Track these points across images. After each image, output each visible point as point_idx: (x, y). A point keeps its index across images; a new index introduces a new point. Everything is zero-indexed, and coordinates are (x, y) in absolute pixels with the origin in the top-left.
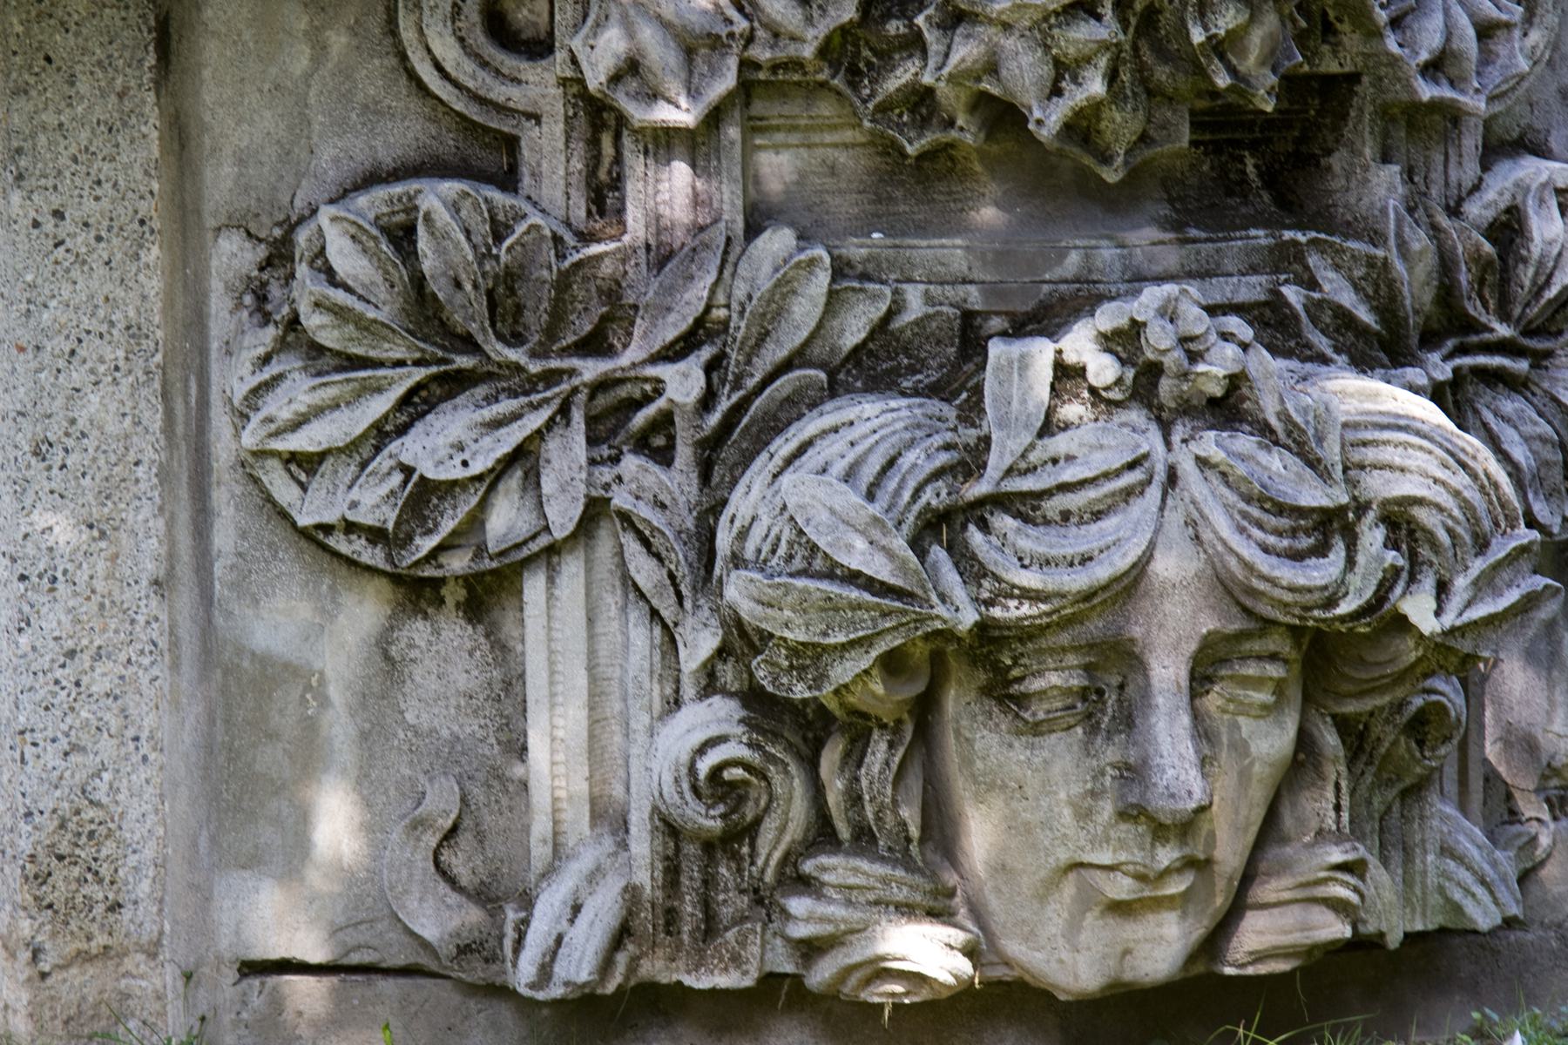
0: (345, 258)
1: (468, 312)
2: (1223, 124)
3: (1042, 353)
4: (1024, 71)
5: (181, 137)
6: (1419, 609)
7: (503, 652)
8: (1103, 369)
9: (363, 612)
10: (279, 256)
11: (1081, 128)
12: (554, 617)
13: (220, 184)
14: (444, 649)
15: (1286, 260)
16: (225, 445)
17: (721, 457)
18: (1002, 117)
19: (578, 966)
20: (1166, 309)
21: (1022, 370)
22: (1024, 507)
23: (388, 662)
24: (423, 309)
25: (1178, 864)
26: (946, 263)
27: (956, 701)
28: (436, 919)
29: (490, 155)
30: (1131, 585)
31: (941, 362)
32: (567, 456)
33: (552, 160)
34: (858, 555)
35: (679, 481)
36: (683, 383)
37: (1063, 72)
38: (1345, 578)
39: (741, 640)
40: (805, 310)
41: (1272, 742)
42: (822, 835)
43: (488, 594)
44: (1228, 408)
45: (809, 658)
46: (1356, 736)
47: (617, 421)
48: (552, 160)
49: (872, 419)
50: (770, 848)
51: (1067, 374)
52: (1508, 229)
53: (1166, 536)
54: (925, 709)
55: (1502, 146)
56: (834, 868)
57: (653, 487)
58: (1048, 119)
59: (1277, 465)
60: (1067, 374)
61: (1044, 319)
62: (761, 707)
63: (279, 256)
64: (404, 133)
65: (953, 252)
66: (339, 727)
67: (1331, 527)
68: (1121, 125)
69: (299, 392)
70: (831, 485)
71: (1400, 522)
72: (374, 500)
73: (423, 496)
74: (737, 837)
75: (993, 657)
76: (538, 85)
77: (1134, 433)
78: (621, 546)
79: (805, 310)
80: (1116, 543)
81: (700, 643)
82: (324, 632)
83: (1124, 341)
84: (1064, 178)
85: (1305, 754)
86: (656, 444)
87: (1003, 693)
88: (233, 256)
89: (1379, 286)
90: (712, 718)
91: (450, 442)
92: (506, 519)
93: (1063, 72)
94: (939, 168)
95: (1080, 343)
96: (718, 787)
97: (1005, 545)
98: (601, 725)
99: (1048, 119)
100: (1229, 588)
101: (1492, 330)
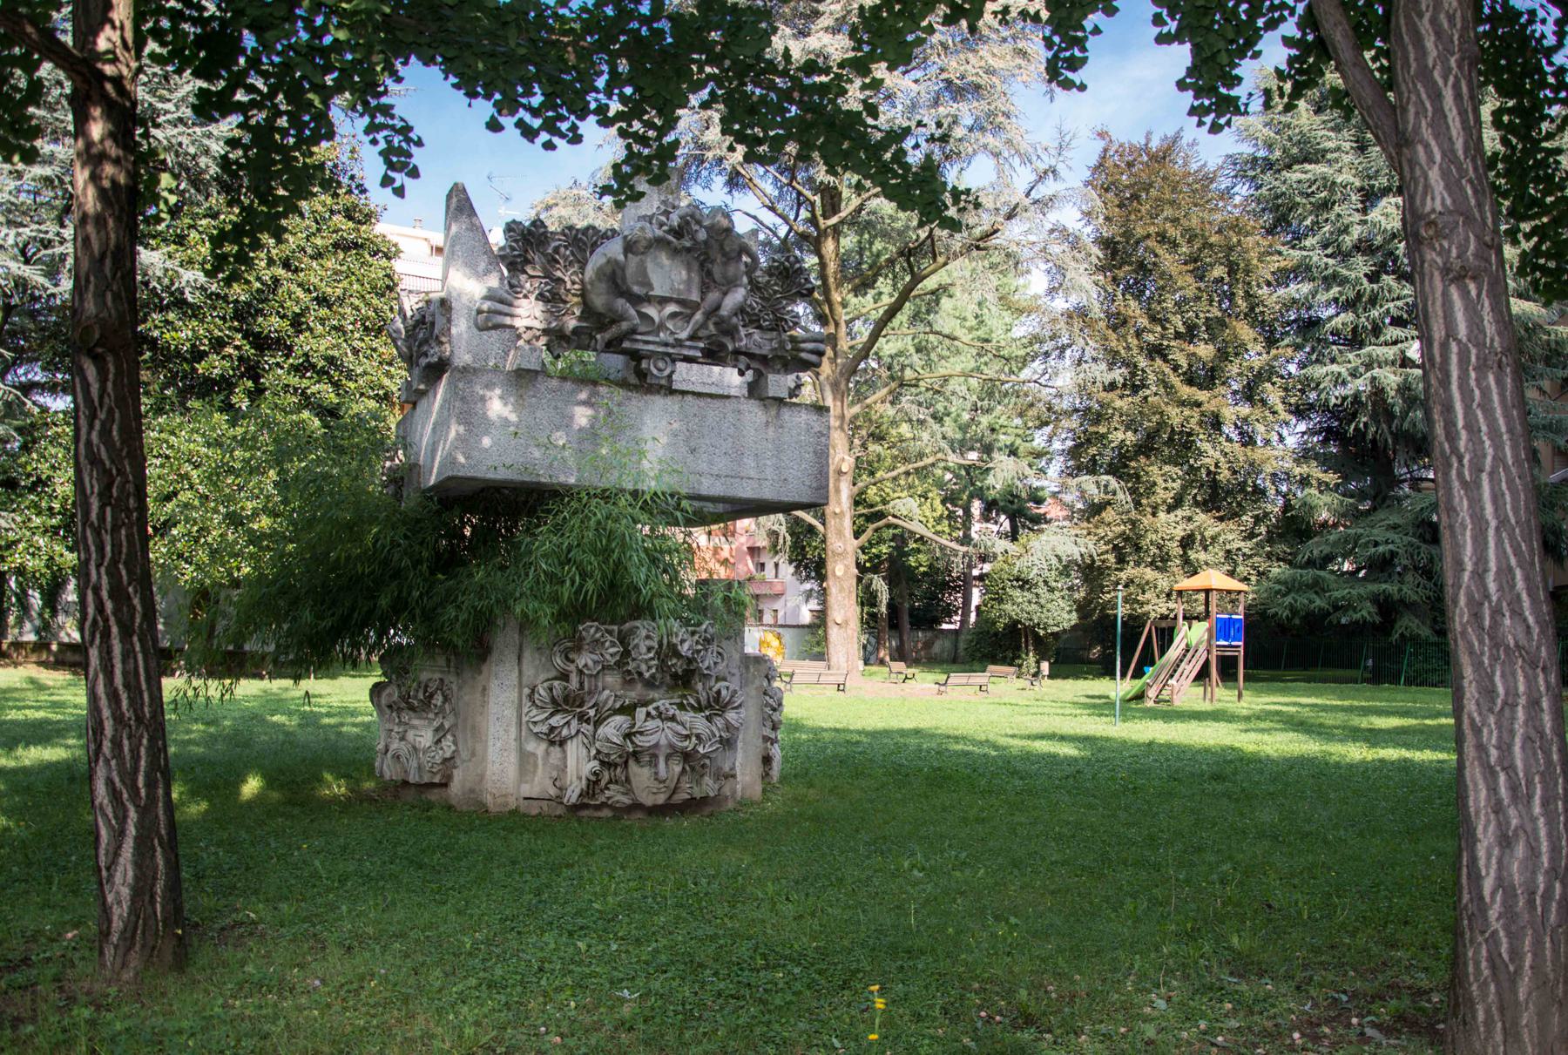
0: (542, 692)
1: (560, 700)
2: (675, 676)
3: (644, 710)
4: (643, 667)
5: (520, 672)
6: (701, 750)
7: (564, 752)
8: (654, 713)
9: (544, 746)
10: (533, 691)
11: (653, 676)
12: (573, 748)
13: (525, 680)
14: (556, 750)
15: (684, 696)
16: (525, 719)
17: (598, 723)
18: (640, 674)
19: (573, 800)
20: (663, 704)
21: (641, 713)
22: (641, 733)
23: (547, 753)
24: (554, 701)
25: (439, 610)
26: (632, 695)
27: (631, 763)
28: (553, 792)
29: (564, 677)
30: (657, 745)
31: (628, 710)
32: (574, 723)
33: (574, 679)
34: (615, 740)
35: (591, 727)
36: (592, 713)
37: (649, 668)
38: (689, 745)
39: (598, 752)
40: (610, 702)
41: (678, 769)
42: (610, 782)
43: (562, 743)
44: (673, 719)
45: (608, 755)
46: (693, 769)
47: (583, 718)
48: (574, 679)
49: (619, 719)
50: (603, 783)
51: (648, 714)
52: (719, 692)
53: (657, 734)
54: (626, 763)
55: (718, 679)
56: (612, 786)
57: (587, 728)
58: (647, 675)
59: (679, 728)
60: (648, 714)
61: (645, 704)
62: (602, 763)
63: (533, 691)
64: (553, 674)
65: (633, 694)
66: (540, 762)
67: (687, 737)
68: (658, 676)
69: (534, 712)
70: (612, 729)
71: (698, 737)
72: (545, 729)
73: (552, 729)
74: (597, 782)
75: (636, 755)
76: (572, 667)
77: (658, 722)
78: (775, 399)
79: (610, 702)
80: (652, 740)
81: (593, 752)
82: (538, 748)
83: (657, 708)
84: (650, 684)
85: (684, 771)
86: (588, 721)
87: (637, 761)
88: (526, 691)
89: (699, 702)
90: (595, 764)
91: (557, 720)
92: (565, 732)
93: (649, 668)
94: (632, 681)
95: (650, 708)
96: (595, 773)
97: (638, 740)
98: (578, 763)
99: (647, 675)
100: (671, 746)
101: (1468, 587)
